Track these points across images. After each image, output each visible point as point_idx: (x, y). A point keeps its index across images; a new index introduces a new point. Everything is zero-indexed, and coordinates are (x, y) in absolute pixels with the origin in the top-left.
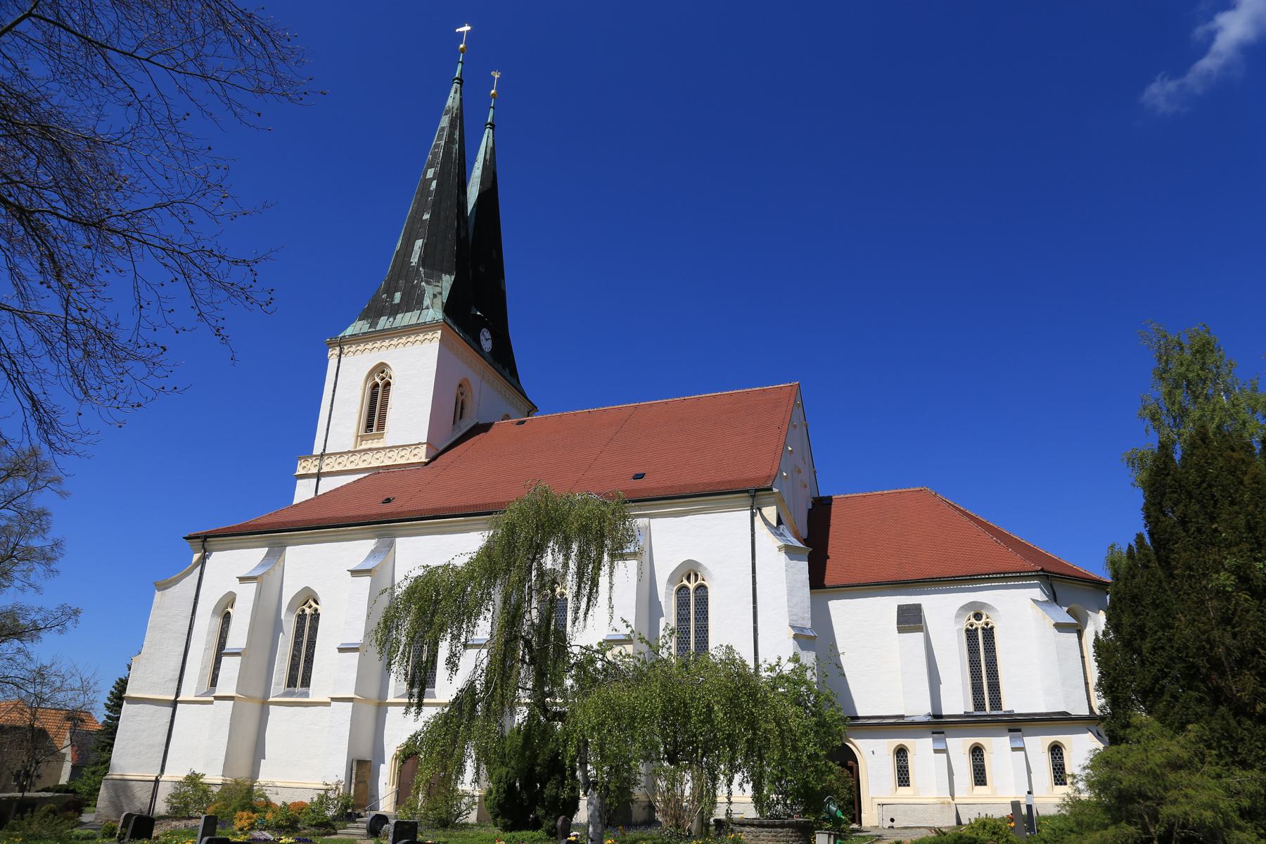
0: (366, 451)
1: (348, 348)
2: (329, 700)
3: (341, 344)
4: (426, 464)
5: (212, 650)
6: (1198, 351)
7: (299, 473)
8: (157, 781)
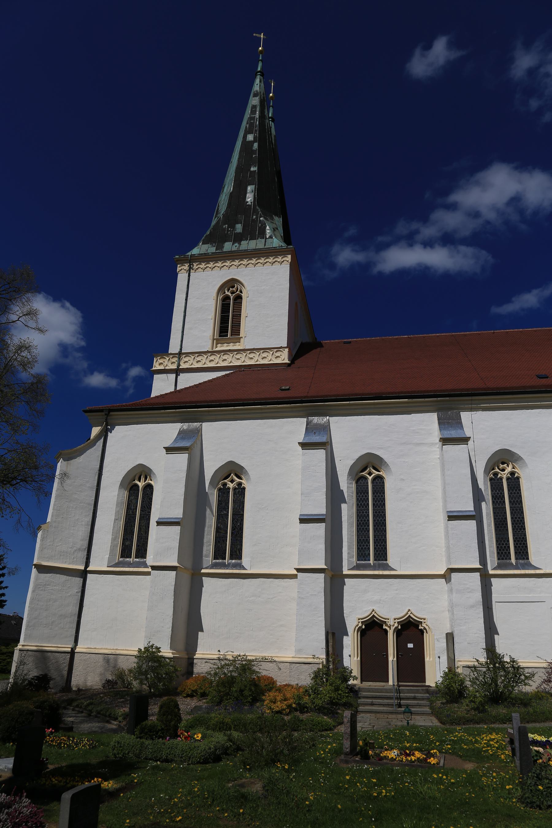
0: (219, 352)
1: (197, 265)
2: (295, 572)
3: (191, 260)
4: (289, 365)
5: (120, 521)
6: (17, 441)
7: (155, 368)
8: (72, 653)
